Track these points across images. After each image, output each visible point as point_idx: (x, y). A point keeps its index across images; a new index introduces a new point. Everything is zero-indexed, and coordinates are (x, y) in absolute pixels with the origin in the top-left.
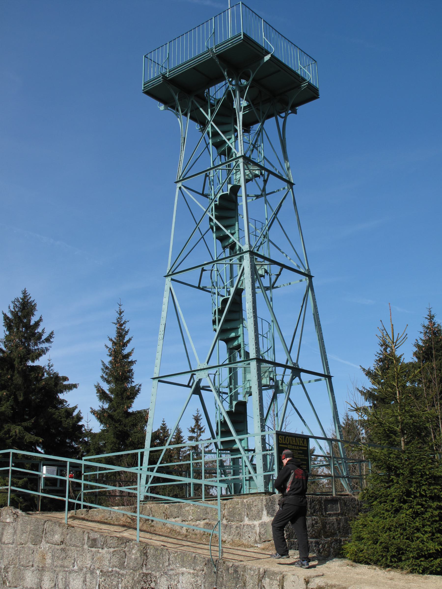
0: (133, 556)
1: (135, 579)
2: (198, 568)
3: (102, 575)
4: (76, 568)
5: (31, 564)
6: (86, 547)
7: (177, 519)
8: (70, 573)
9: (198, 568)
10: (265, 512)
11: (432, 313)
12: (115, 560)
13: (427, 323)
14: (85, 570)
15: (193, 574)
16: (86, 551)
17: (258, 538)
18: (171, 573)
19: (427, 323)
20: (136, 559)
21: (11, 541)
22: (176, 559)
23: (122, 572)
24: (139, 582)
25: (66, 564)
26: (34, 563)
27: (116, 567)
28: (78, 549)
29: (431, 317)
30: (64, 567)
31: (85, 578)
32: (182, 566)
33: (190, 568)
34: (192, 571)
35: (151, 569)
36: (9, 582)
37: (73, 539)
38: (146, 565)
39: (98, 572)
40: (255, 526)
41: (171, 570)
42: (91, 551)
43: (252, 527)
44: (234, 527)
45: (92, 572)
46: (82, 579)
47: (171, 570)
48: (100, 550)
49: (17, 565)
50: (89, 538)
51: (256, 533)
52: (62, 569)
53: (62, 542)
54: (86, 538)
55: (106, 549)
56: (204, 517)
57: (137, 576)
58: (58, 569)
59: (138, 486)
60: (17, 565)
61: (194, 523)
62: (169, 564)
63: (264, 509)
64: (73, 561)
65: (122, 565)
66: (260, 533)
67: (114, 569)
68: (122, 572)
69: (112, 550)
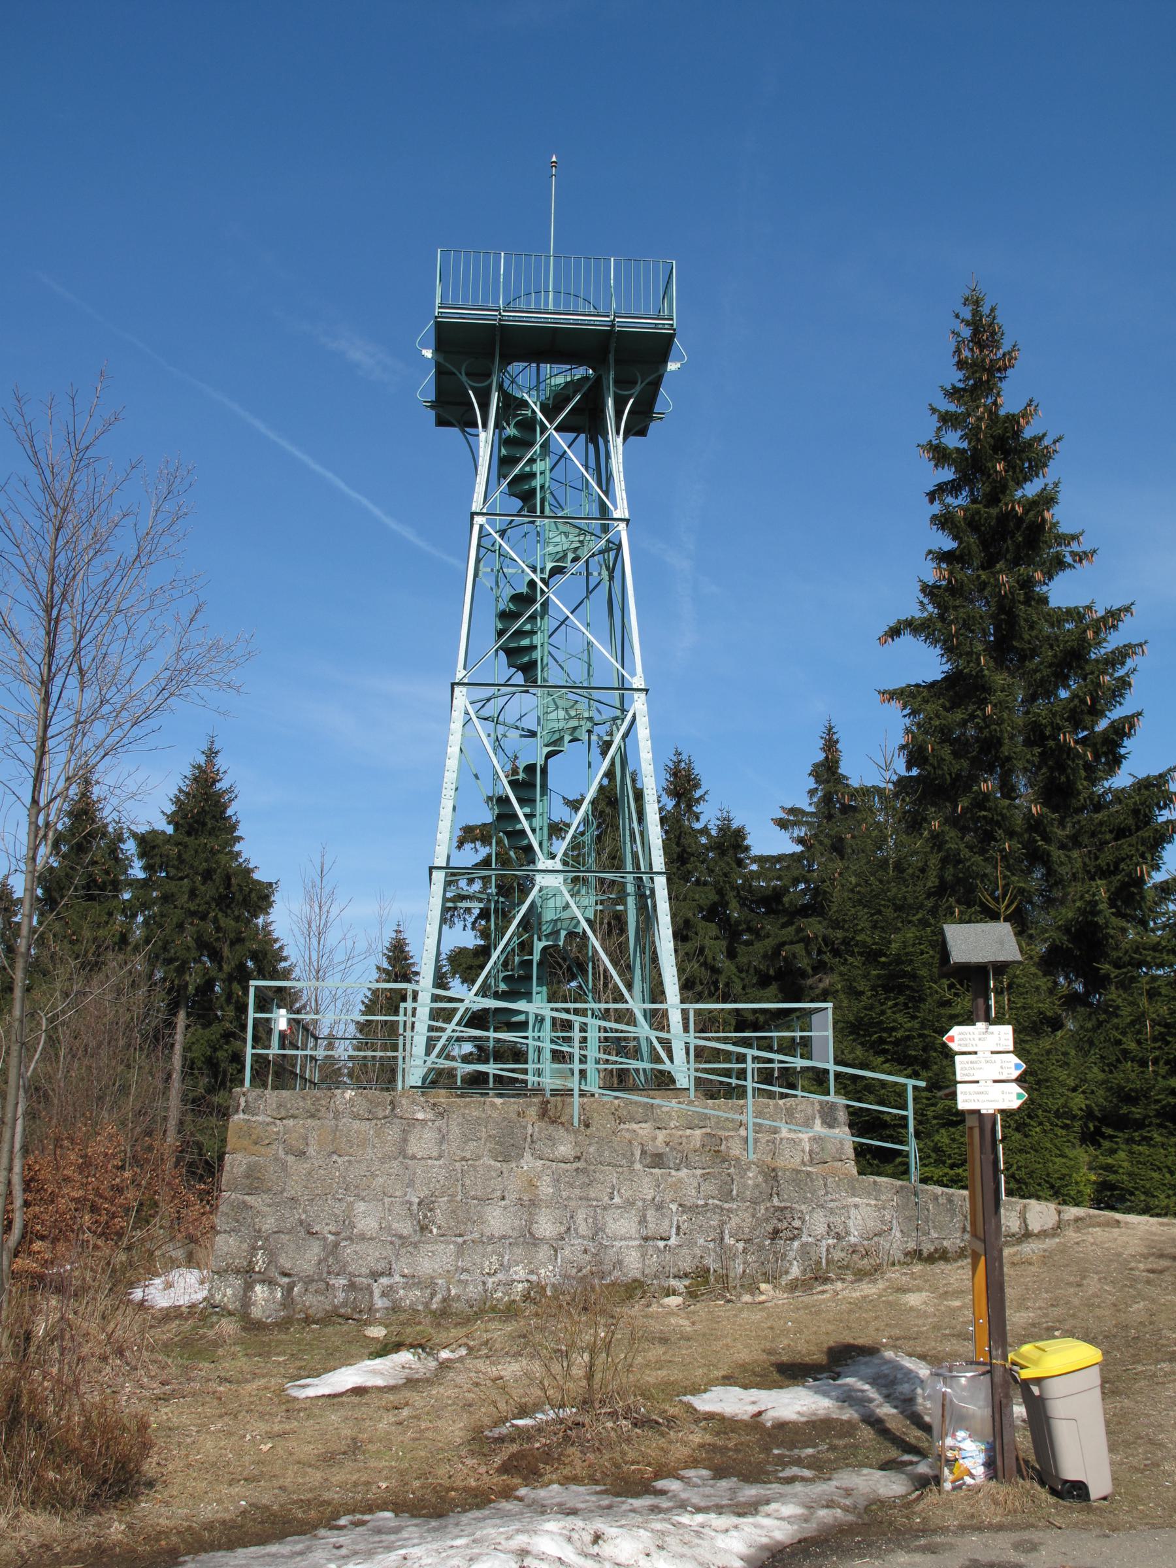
0: (750, 1182)
1: (759, 1215)
2: (883, 1198)
3: (683, 1212)
4: (617, 1200)
5: (498, 1194)
6: (638, 1166)
7: (643, 1125)
8: (605, 1209)
9: (883, 1198)
10: (818, 1121)
11: (216, 747)
12: (710, 1188)
13: (202, 760)
14: (640, 1204)
15: (876, 1206)
16: (641, 1173)
17: (807, 1158)
18: (832, 1205)
19: (202, 760)
20: (757, 1186)
21: (435, 1154)
22: (838, 1186)
23: (726, 1206)
24: (767, 1220)
25: (592, 1195)
26: (506, 1194)
27: (713, 1198)
28: (620, 1169)
29: (211, 754)
30: (588, 1199)
31: (644, 1216)
32: (854, 1195)
33: (869, 1195)
34: (873, 1202)
35: (790, 1199)
36: (439, 1228)
37: (606, 1154)
38: (778, 1195)
39: (674, 1207)
40: (801, 1140)
41: (832, 1200)
42: (651, 1174)
43: (795, 1142)
44: (764, 1141)
45: (659, 1207)
46: (637, 1219)
47: (832, 1200)
48: (673, 1172)
49: (459, 1198)
50: (643, 1152)
51: (803, 1151)
52: (584, 1202)
53: (578, 1158)
54: (638, 1153)
55: (685, 1170)
56: (702, 1124)
57: (763, 1211)
58: (572, 1204)
59: (693, 1074)
60: (459, 1198)
61: (680, 1133)
62: (827, 1193)
63: (817, 1116)
64: (609, 1190)
65: (727, 1196)
66: (811, 1151)
67: (710, 1201)
68: (726, 1206)
69: (699, 1172)
